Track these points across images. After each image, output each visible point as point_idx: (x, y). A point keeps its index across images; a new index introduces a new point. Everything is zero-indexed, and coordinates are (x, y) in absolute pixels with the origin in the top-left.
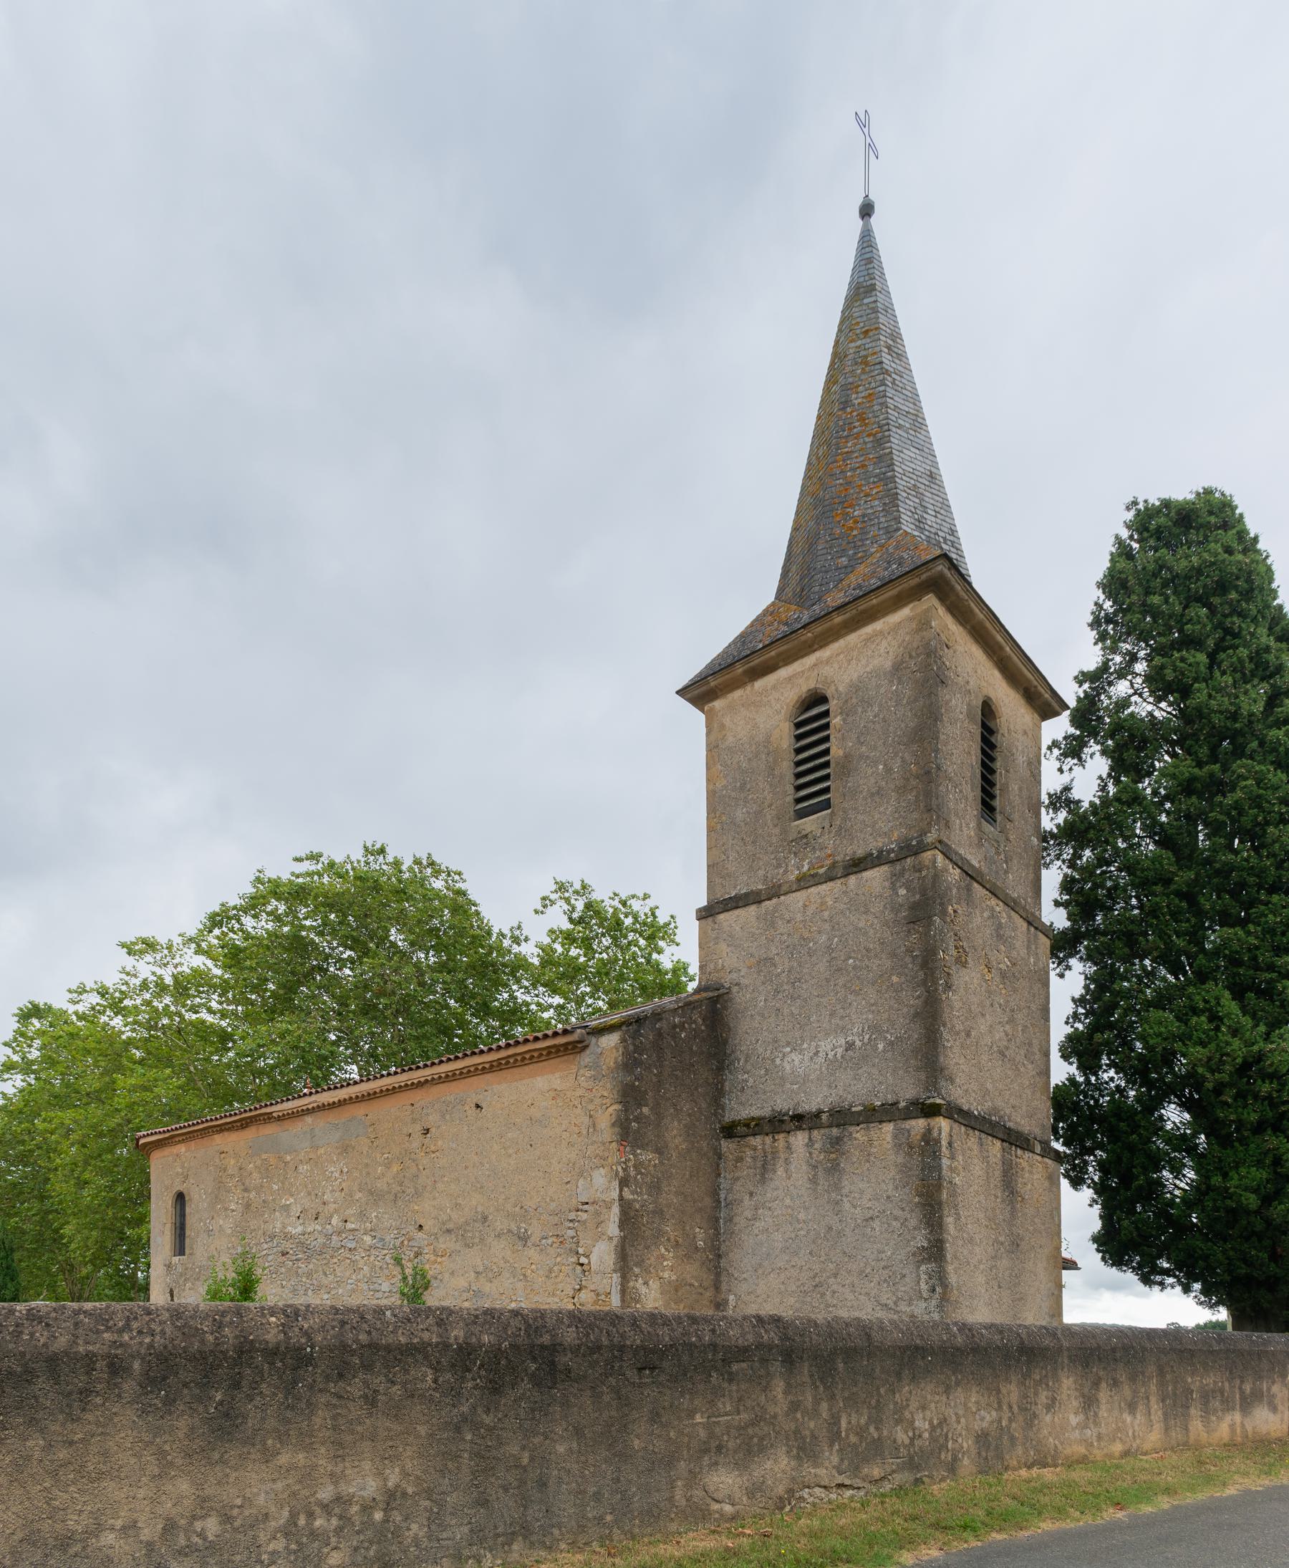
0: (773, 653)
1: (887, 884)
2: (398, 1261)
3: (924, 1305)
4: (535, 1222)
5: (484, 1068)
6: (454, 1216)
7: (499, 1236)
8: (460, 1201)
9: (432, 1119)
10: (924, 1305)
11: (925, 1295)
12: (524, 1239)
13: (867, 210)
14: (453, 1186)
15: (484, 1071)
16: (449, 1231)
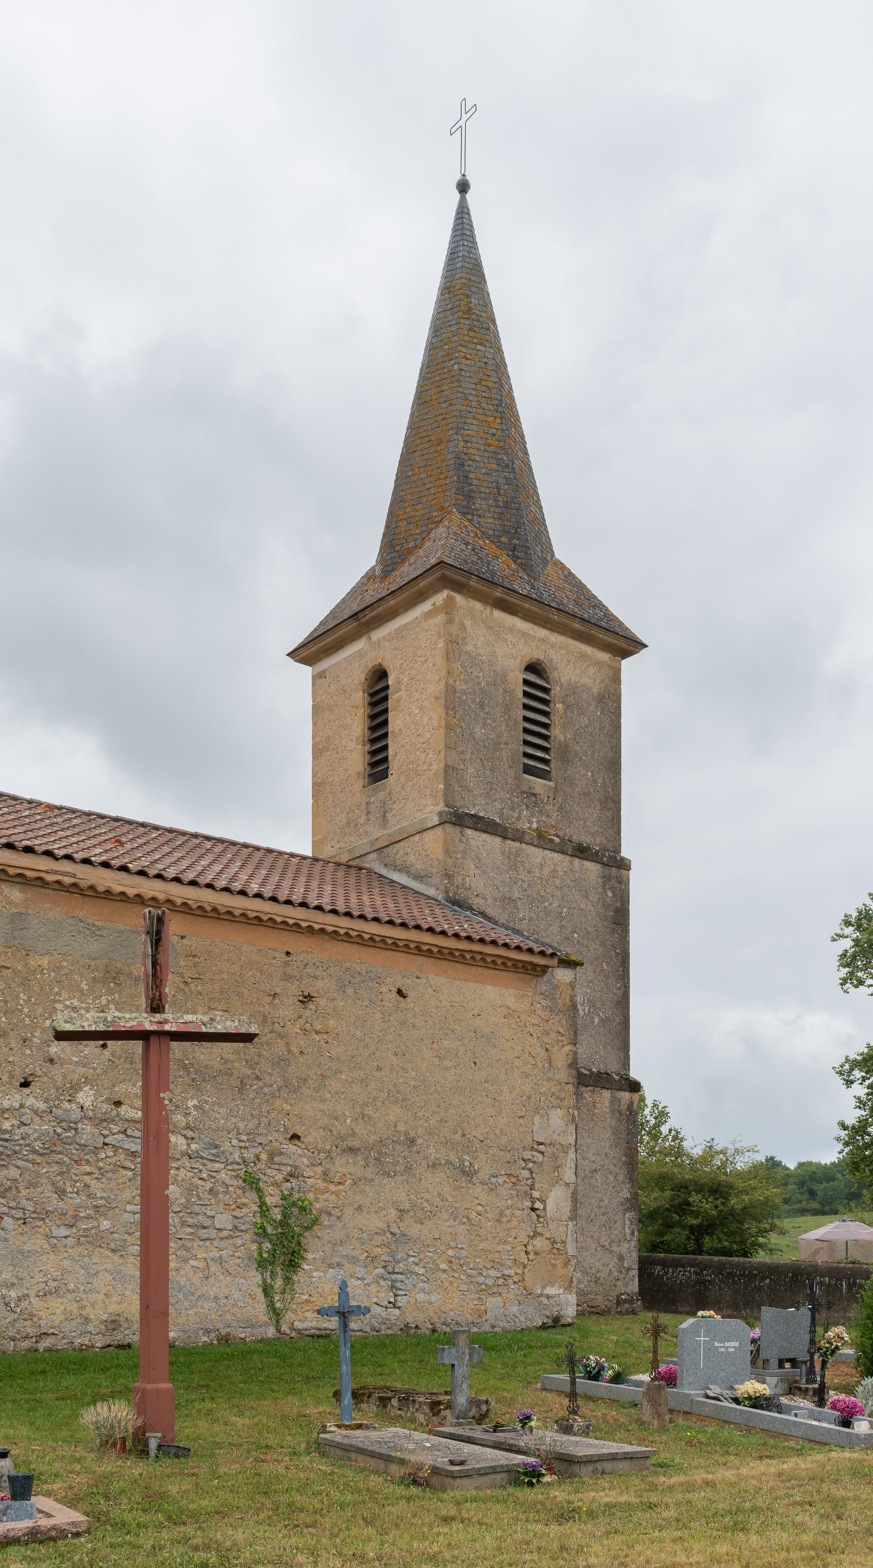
0: (527, 606)
1: (600, 881)
2: (252, 1183)
3: (627, 1246)
4: (482, 1156)
5: (429, 950)
6: (360, 1129)
7: (434, 1166)
8: (369, 1111)
9: (323, 986)
10: (627, 1246)
11: (628, 1238)
12: (469, 1174)
13: (463, 187)
14: (356, 1089)
15: (419, 950)
16: (351, 1150)
